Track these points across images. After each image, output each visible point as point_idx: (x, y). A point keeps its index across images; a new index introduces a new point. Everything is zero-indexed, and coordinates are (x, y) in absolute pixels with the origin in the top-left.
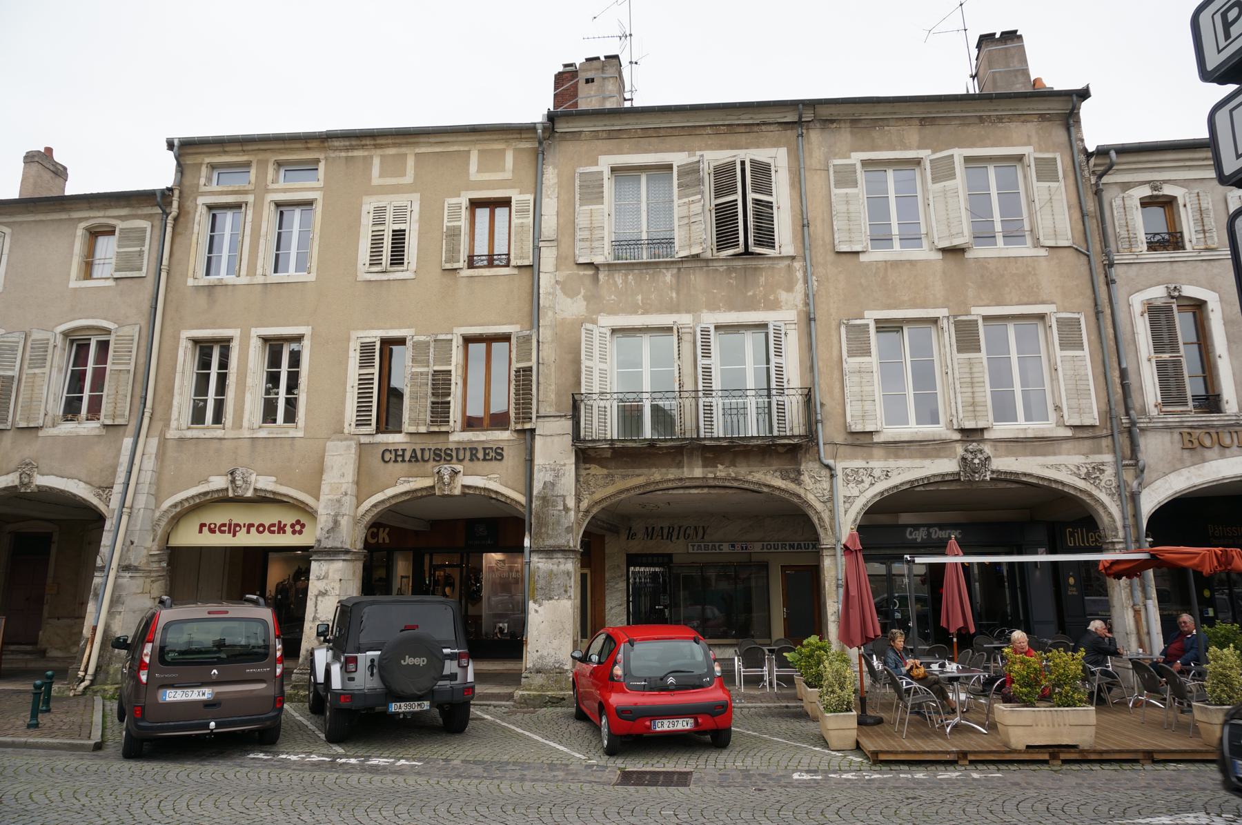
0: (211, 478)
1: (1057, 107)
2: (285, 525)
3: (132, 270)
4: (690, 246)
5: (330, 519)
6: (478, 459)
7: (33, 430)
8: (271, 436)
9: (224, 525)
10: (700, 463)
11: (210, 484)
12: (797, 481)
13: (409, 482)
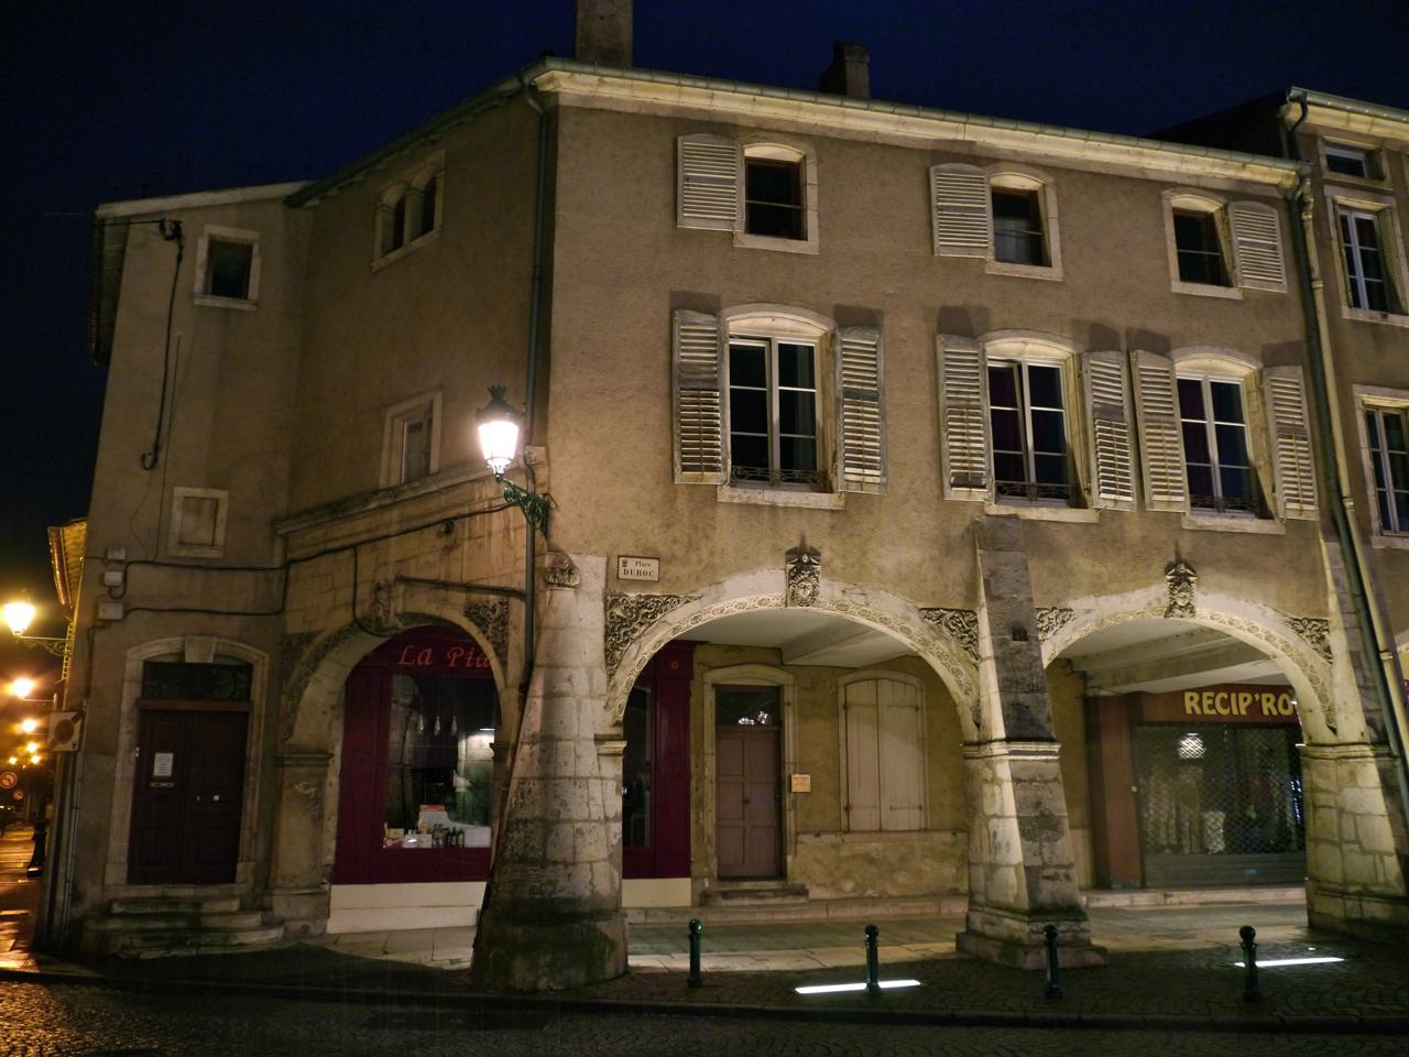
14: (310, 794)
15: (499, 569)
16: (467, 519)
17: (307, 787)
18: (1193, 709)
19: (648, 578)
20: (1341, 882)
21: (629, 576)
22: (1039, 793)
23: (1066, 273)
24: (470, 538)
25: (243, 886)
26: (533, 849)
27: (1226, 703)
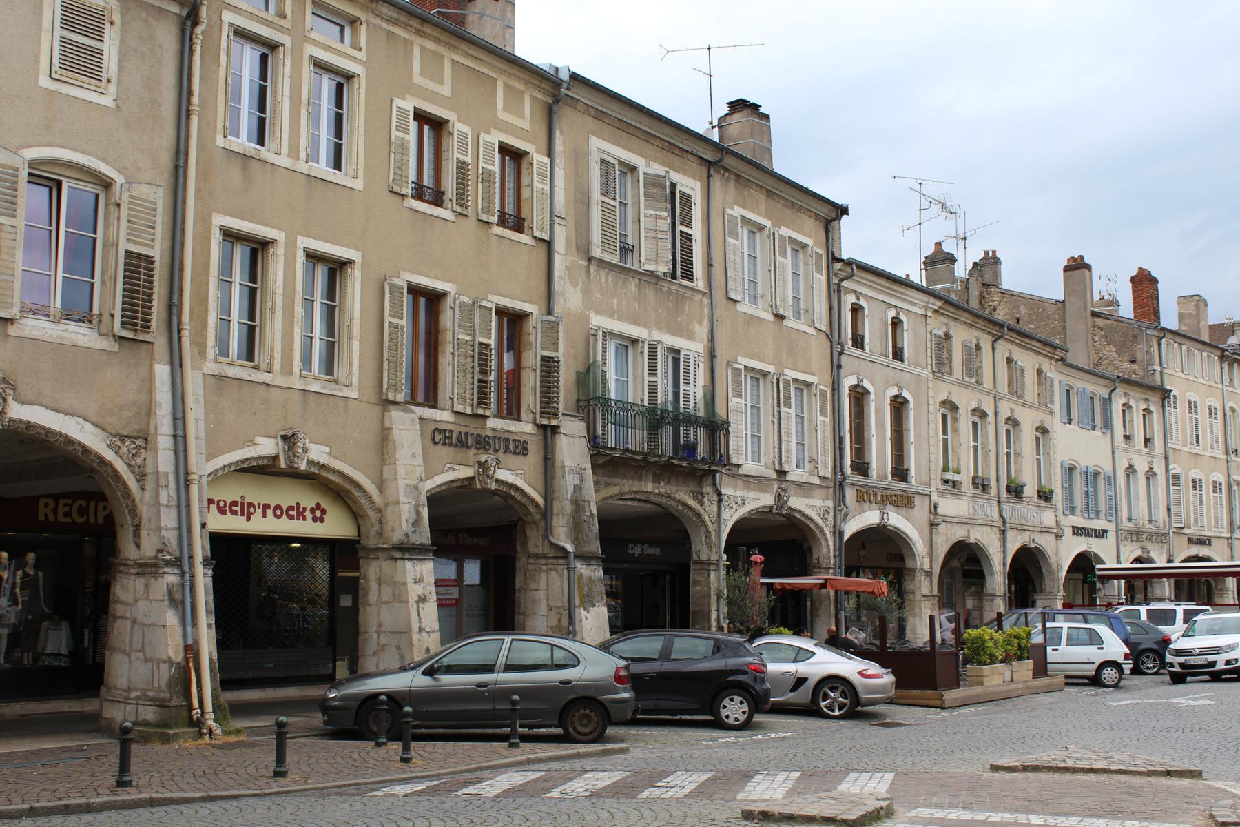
0: (258, 440)
1: (825, 211)
2: (304, 509)
4: (656, 262)
5: (413, 510)
8: (325, 391)
12: (701, 503)
13: (454, 470)
18: (46, 515)
20: (126, 688)
27: (83, 511)
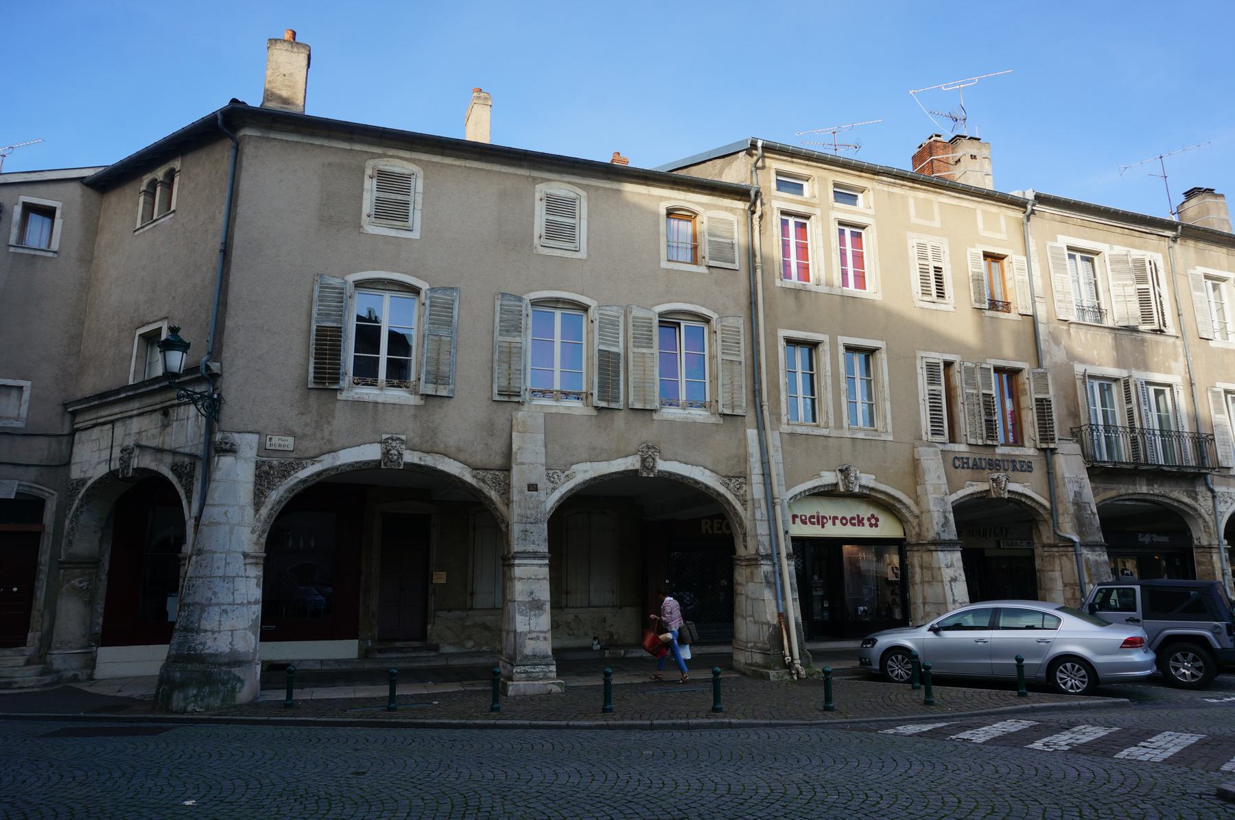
2: (863, 519)
3: (725, 261)
6: (1018, 470)
7: (647, 413)
8: (868, 438)
9: (813, 517)
10: (1145, 482)
11: (822, 479)
12: (1196, 499)
14: (84, 586)
15: (191, 441)
16: (176, 408)
17: (80, 582)
19: (286, 449)
21: (273, 448)
22: (533, 587)
23: (589, 255)
24: (177, 420)
25: (31, 648)
26: (192, 622)
